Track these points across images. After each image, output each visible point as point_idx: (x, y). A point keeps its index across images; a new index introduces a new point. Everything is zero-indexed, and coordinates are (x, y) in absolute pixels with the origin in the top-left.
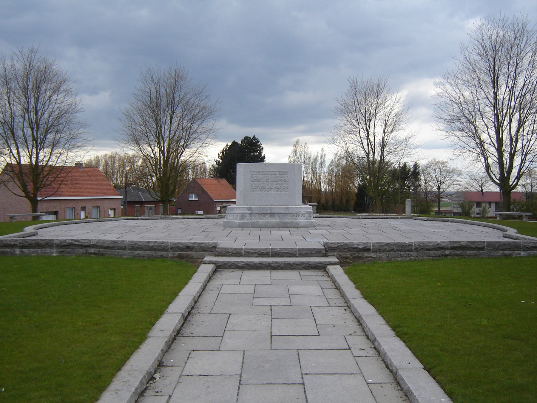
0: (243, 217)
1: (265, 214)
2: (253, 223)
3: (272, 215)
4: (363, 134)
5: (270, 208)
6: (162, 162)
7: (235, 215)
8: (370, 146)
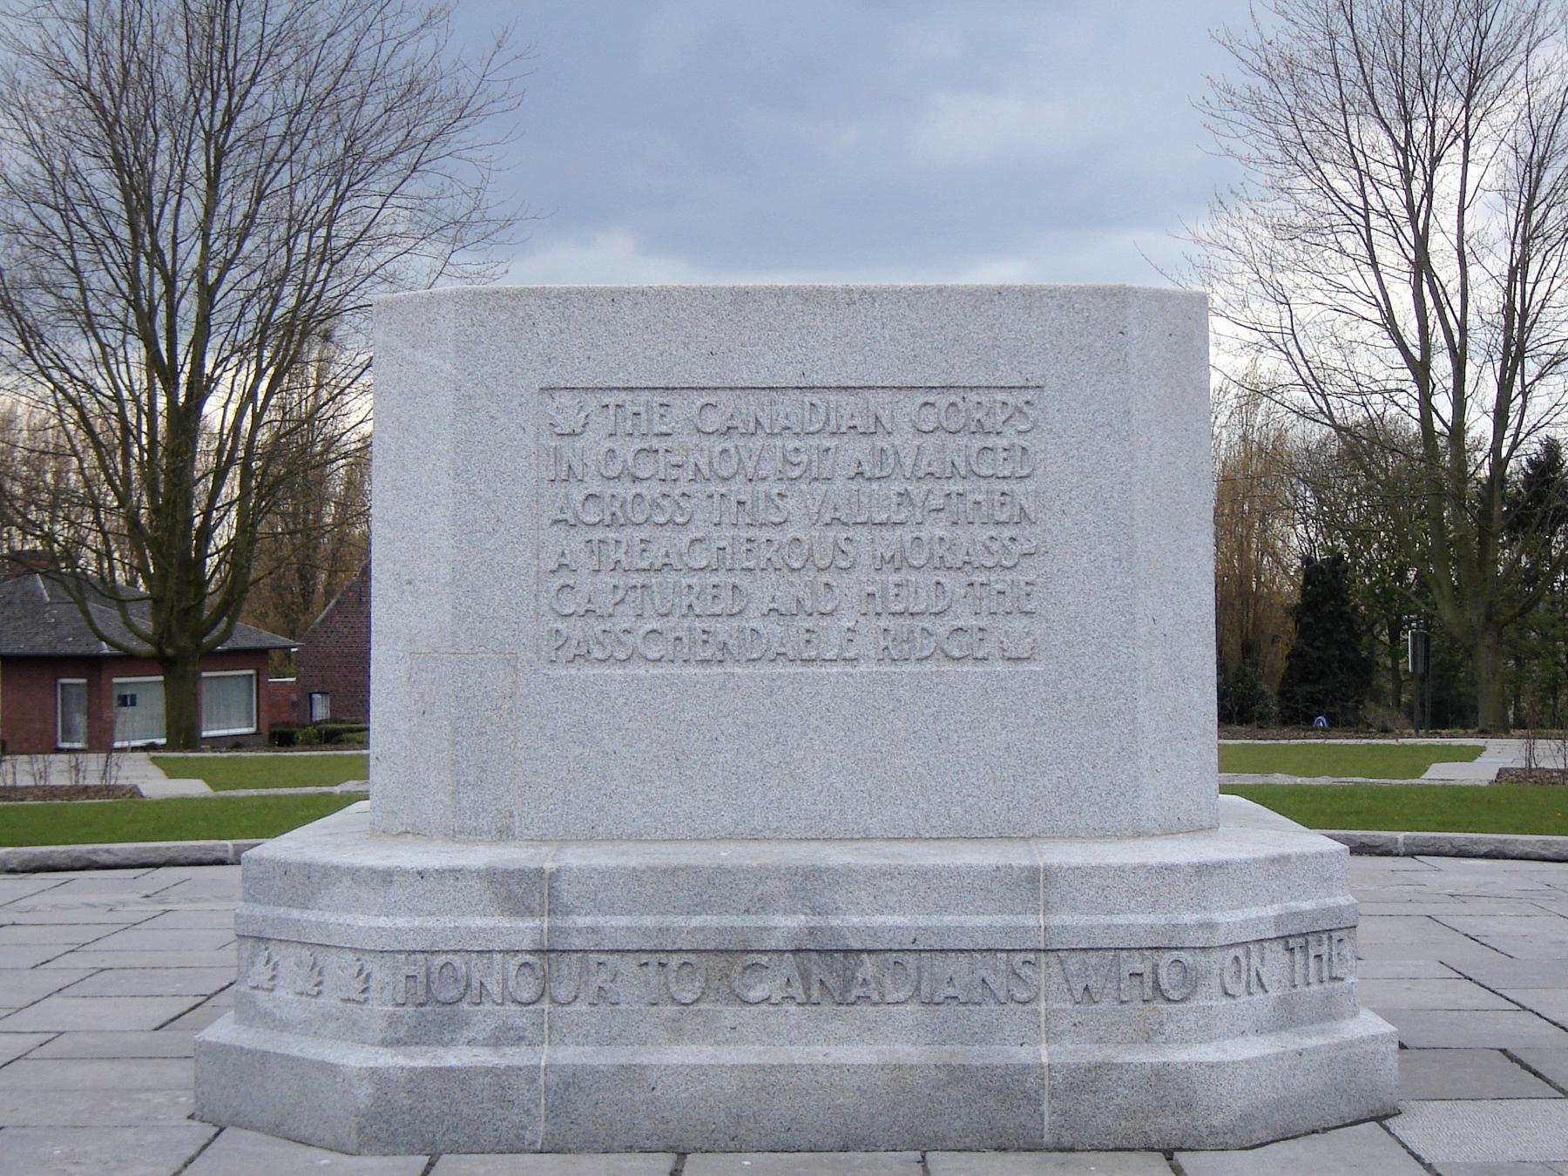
0: (435, 995)
1: (732, 959)
2: (570, 1082)
3: (831, 969)
4: (1391, 255)
5: (808, 885)
6: (161, 423)
7: (340, 968)
8: (1432, 314)
